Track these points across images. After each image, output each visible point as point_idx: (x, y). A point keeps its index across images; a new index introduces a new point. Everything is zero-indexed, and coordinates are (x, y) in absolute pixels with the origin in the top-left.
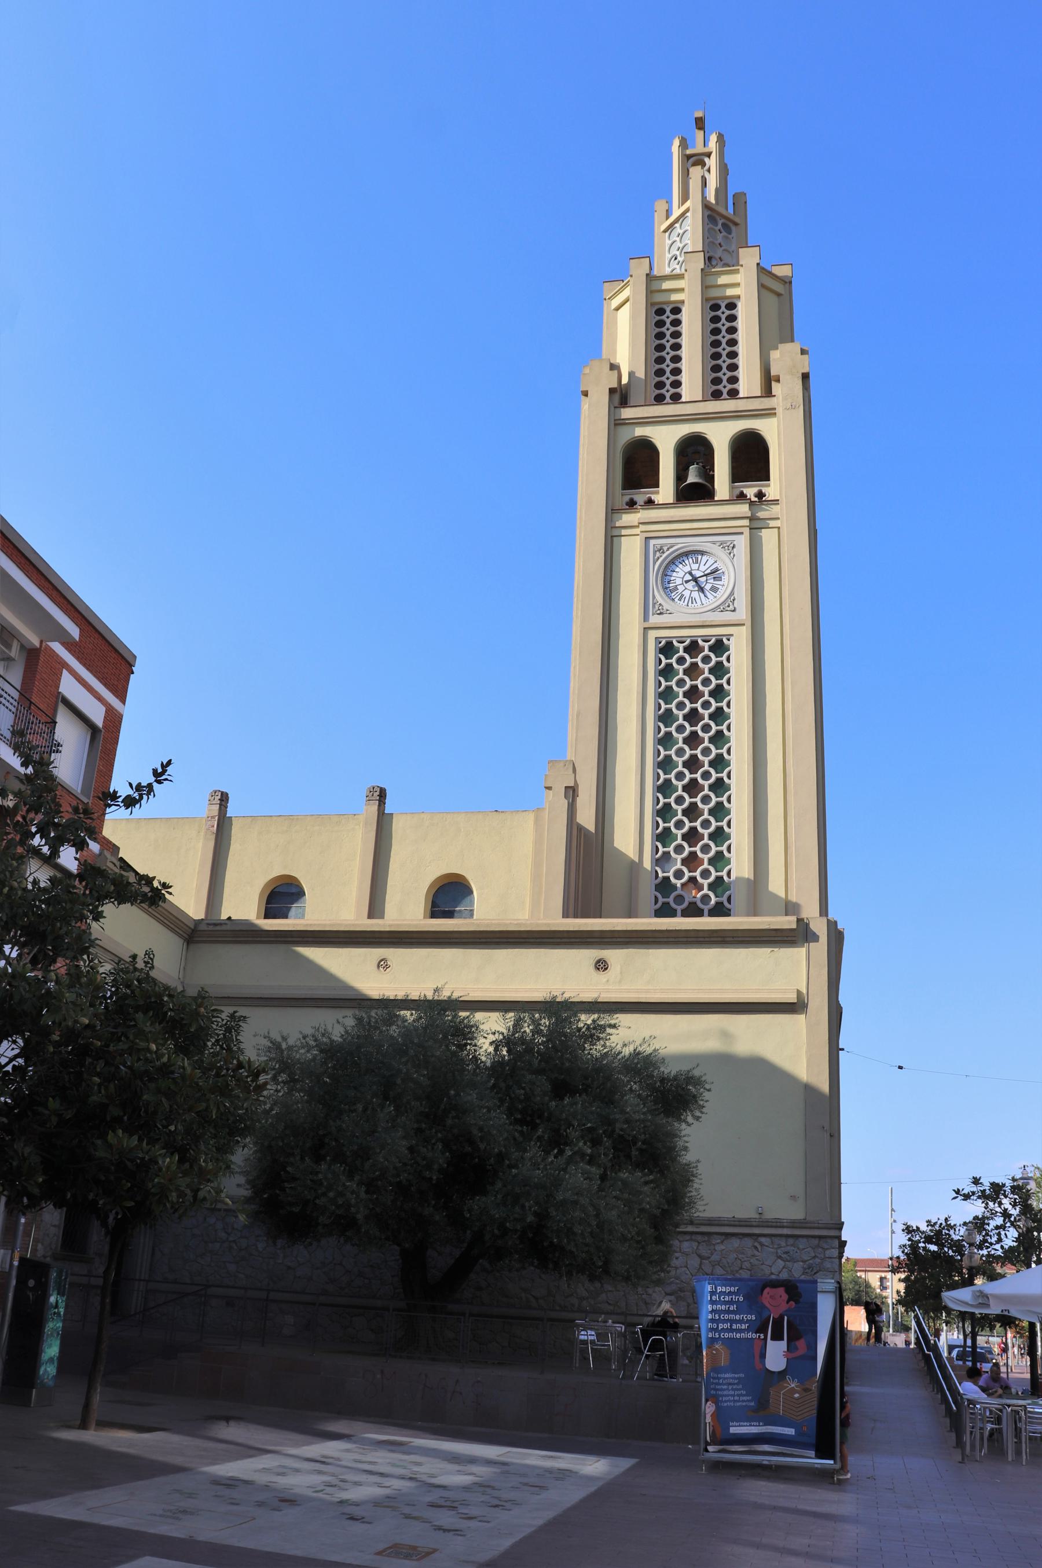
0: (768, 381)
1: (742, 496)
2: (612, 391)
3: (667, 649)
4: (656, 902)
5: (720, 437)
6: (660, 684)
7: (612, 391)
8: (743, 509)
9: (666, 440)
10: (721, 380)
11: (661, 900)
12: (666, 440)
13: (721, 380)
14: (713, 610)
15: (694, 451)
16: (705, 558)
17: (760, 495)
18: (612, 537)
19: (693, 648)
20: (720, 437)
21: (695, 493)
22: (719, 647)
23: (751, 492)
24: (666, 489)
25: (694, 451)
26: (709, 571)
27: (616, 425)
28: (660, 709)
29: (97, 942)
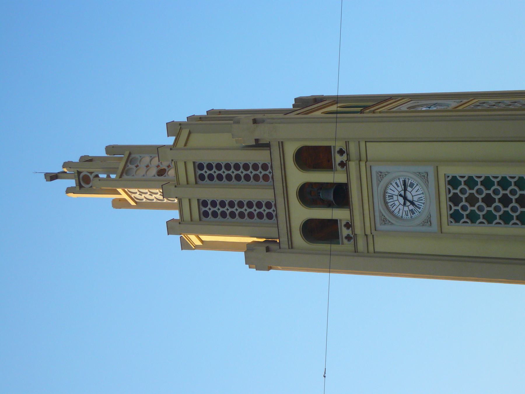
0: (258, 145)
1: (342, 164)
2: (268, 250)
3: (456, 217)
4: (499, 223)
5: (297, 177)
6: (515, 224)
7: (268, 250)
8: (352, 165)
9: (301, 213)
10: (259, 174)
11: (481, 220)
12: (301, 213)
13: (259, 174)
14: (427, 187)
15: (309, 195)
16: (389, 191)
17: (341, 152)
18: (374, 252)
19: (455, 200)
20: (297, 177)
21: (340, 195)
22: (453, 182)
23: (338, 159)
24: (340, 214)
25: (309, 195)
26: (403, 187)
27: (292, 248)
28: (499, 223)
29: (72, 183)
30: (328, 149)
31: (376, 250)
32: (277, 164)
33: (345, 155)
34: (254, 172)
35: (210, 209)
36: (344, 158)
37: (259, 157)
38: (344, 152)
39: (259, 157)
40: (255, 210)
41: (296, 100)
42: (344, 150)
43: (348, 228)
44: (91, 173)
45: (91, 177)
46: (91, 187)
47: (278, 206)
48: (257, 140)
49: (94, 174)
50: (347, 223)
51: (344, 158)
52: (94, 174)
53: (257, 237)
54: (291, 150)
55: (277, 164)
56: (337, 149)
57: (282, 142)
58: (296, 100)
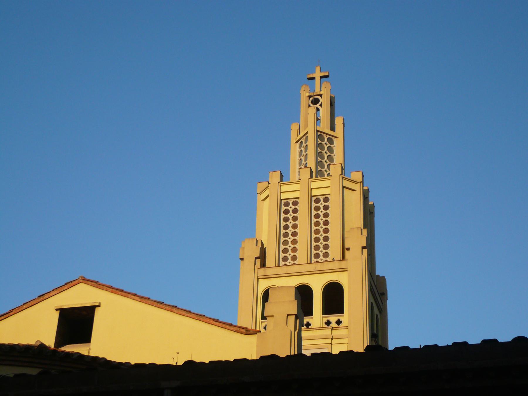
0: (344, 249)
8: (328, 332)
10: (318, 251)
17: (339, 322)
33: (336, 325)
34: (321, 246)
35: (321, 243)
37: (335, 251)
38: (339, 325)
39: (335, 251)
41: (384, 277)
42: (341, 325)
43: (326, 323)
44: (321, 105)
45: (318, 106)
46: (309, 106)
48: (348, 249)
49: (319, 107)
50: (310, 325)
52: (319, 107)
54: (342, 278)
56: (341, 319)
58: (384, 277)
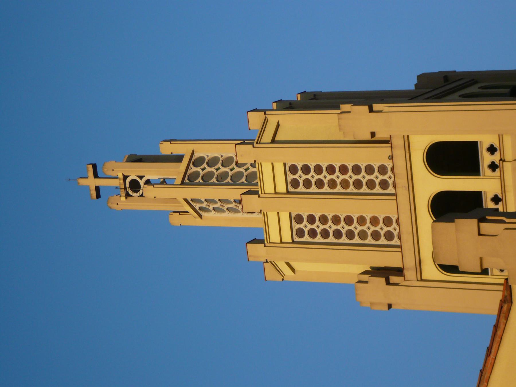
0: (373, 140)
10: (376, 182)
13: (376, 182)
17: (492, 150)
25: (446, 207)
30: (473, 146)
31: (423, 278)
32: (405, 220)
36: (496, 158)
37: (376, 156)
39: (376, 156)
40: (369, 228)
42: (496, 145)
44: (141, 177)
45: (142, 182)
47: (403, 236)
49: (144, 179)
51: (496, 158)
52: (144, 179)
53: (88, 171)
54: (421, 144)
55: (405, 220)
56: (486, 145)
57: (408, 136)
